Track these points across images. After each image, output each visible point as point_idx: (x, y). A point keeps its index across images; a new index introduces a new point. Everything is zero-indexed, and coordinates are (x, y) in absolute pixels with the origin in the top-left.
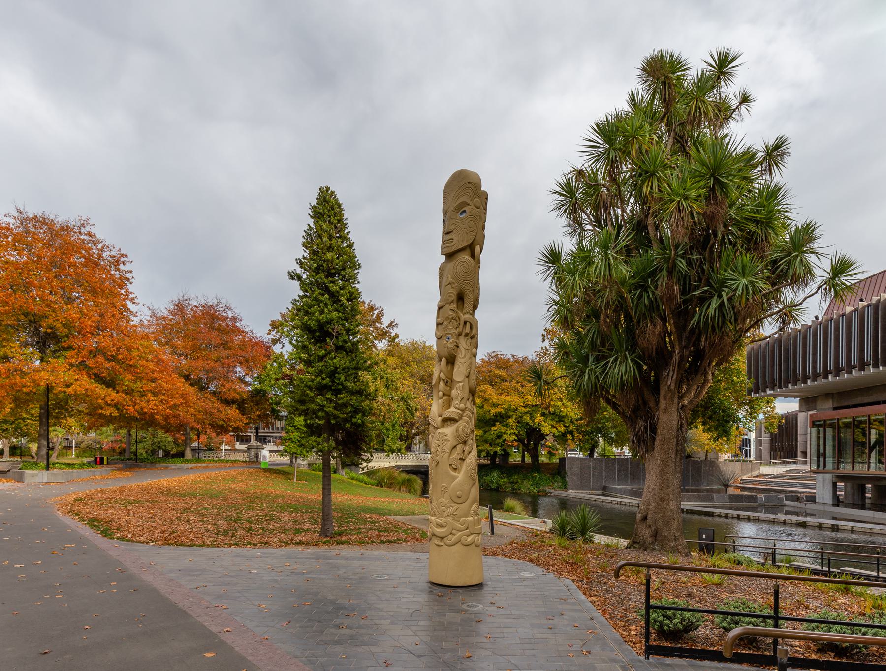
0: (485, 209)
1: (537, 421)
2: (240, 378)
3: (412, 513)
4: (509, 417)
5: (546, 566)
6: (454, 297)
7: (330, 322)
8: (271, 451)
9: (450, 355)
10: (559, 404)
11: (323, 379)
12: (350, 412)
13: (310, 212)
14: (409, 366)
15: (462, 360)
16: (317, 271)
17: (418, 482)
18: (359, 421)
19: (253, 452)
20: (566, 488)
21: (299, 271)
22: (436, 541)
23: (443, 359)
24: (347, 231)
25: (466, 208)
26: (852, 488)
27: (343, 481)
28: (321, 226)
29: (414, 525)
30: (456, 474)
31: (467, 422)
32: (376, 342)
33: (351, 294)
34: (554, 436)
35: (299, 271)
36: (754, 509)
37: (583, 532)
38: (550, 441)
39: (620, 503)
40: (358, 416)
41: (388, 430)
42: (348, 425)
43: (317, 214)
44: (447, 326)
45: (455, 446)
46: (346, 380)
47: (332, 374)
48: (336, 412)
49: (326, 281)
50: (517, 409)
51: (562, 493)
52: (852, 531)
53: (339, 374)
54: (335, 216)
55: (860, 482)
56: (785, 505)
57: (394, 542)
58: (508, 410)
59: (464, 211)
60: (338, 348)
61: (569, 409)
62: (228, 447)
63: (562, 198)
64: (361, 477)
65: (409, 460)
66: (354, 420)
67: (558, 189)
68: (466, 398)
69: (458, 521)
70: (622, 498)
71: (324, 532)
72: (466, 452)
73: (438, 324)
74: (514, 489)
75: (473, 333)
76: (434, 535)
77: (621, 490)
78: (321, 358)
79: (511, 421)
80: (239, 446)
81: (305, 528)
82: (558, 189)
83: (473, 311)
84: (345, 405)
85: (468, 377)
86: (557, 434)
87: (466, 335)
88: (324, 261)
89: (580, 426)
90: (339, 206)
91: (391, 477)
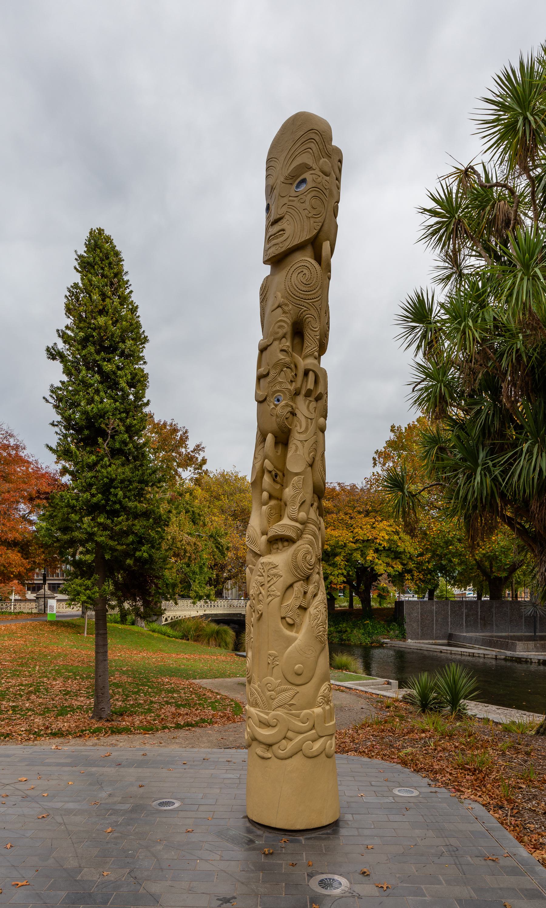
0: (338, 179)
1: (369, 558)
2: (23, 517)
3: (223, 675)
4: (336, 555)
5: (431, 772)
6: (287, 328)
7: (102, 414)
8: (58, 601)
9: (280, 427)
10: (396, 537)
11: (93, 496)
12: (132, 543)
13: (76, 264)
14: (219, 500)
15: (302, 437)
16: (84, 342)
17: (231, 633)
18: (145, 554)
19: (42, 602)
20: (403, 637)
21: (61, 345)
22: (260, 750)
23: (270, 437)
24: (141, 331)
25: (307, 175)
27: (142, 634)
28: (90, 281)
29: (224, 693)
30: (292, 634)
31: (311, 544)
32: (180, 470)
33: (134, 375)
34: (389, 575)
35: (61, 345)
37: (454, 702)
38: (383, 583)
39: (473, 655)
40: (143, 548)
41: (194, 573)
42: (129, 561)
43: (85, 266)
44: (275, 378)
45: (291, 586)
46: (125, 496)
47: (107, 488)
48: (111, 543)
49: (98, 358)
50: (345, 545)
51: (399, 643)
53: (115, 488)
54: (111, 268)
57: (196, 725)
58: (335, 547)
59: (304, 181)
60: (115, 453)
61: (407, 544)
62: (17, 597)
63: (435, 220)
64: (164, 629)
65: (220, 608)
66: (138, 554)
67: (432, 205)
68: (308, 502)
69: (298, 716)
70: (473, 648)
71: (98, 714)
72: (309, 595)
73: (260, 378)
74: (342, 639)
75: (320, 390)
76: (254, 739)
77: (471, 638)
78: (91, 467)
79: (338, 559)
80: (30, 595)
81: (75, 703)
82: (432, 205)
83: (320, 356)
84: (126, 533)
85: (311, 465)
86: (393, 573)
87: (309, 393)
88: (94, 329)
89: (420, 564)
90: (117, 254)
91: (198, 629)
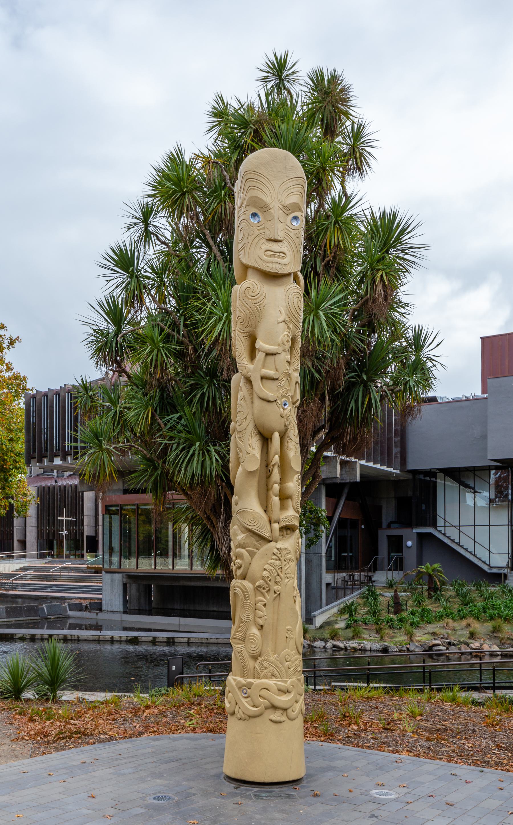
26: (138, 590)
36: (35, 625)
52: (189, 643)
55: (145, 583)
56: (68, 617)
